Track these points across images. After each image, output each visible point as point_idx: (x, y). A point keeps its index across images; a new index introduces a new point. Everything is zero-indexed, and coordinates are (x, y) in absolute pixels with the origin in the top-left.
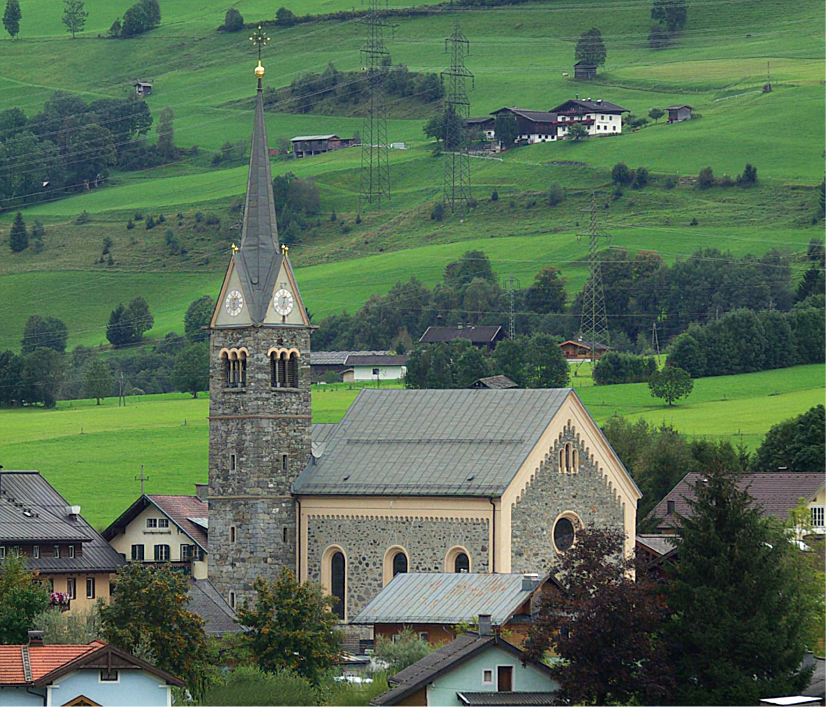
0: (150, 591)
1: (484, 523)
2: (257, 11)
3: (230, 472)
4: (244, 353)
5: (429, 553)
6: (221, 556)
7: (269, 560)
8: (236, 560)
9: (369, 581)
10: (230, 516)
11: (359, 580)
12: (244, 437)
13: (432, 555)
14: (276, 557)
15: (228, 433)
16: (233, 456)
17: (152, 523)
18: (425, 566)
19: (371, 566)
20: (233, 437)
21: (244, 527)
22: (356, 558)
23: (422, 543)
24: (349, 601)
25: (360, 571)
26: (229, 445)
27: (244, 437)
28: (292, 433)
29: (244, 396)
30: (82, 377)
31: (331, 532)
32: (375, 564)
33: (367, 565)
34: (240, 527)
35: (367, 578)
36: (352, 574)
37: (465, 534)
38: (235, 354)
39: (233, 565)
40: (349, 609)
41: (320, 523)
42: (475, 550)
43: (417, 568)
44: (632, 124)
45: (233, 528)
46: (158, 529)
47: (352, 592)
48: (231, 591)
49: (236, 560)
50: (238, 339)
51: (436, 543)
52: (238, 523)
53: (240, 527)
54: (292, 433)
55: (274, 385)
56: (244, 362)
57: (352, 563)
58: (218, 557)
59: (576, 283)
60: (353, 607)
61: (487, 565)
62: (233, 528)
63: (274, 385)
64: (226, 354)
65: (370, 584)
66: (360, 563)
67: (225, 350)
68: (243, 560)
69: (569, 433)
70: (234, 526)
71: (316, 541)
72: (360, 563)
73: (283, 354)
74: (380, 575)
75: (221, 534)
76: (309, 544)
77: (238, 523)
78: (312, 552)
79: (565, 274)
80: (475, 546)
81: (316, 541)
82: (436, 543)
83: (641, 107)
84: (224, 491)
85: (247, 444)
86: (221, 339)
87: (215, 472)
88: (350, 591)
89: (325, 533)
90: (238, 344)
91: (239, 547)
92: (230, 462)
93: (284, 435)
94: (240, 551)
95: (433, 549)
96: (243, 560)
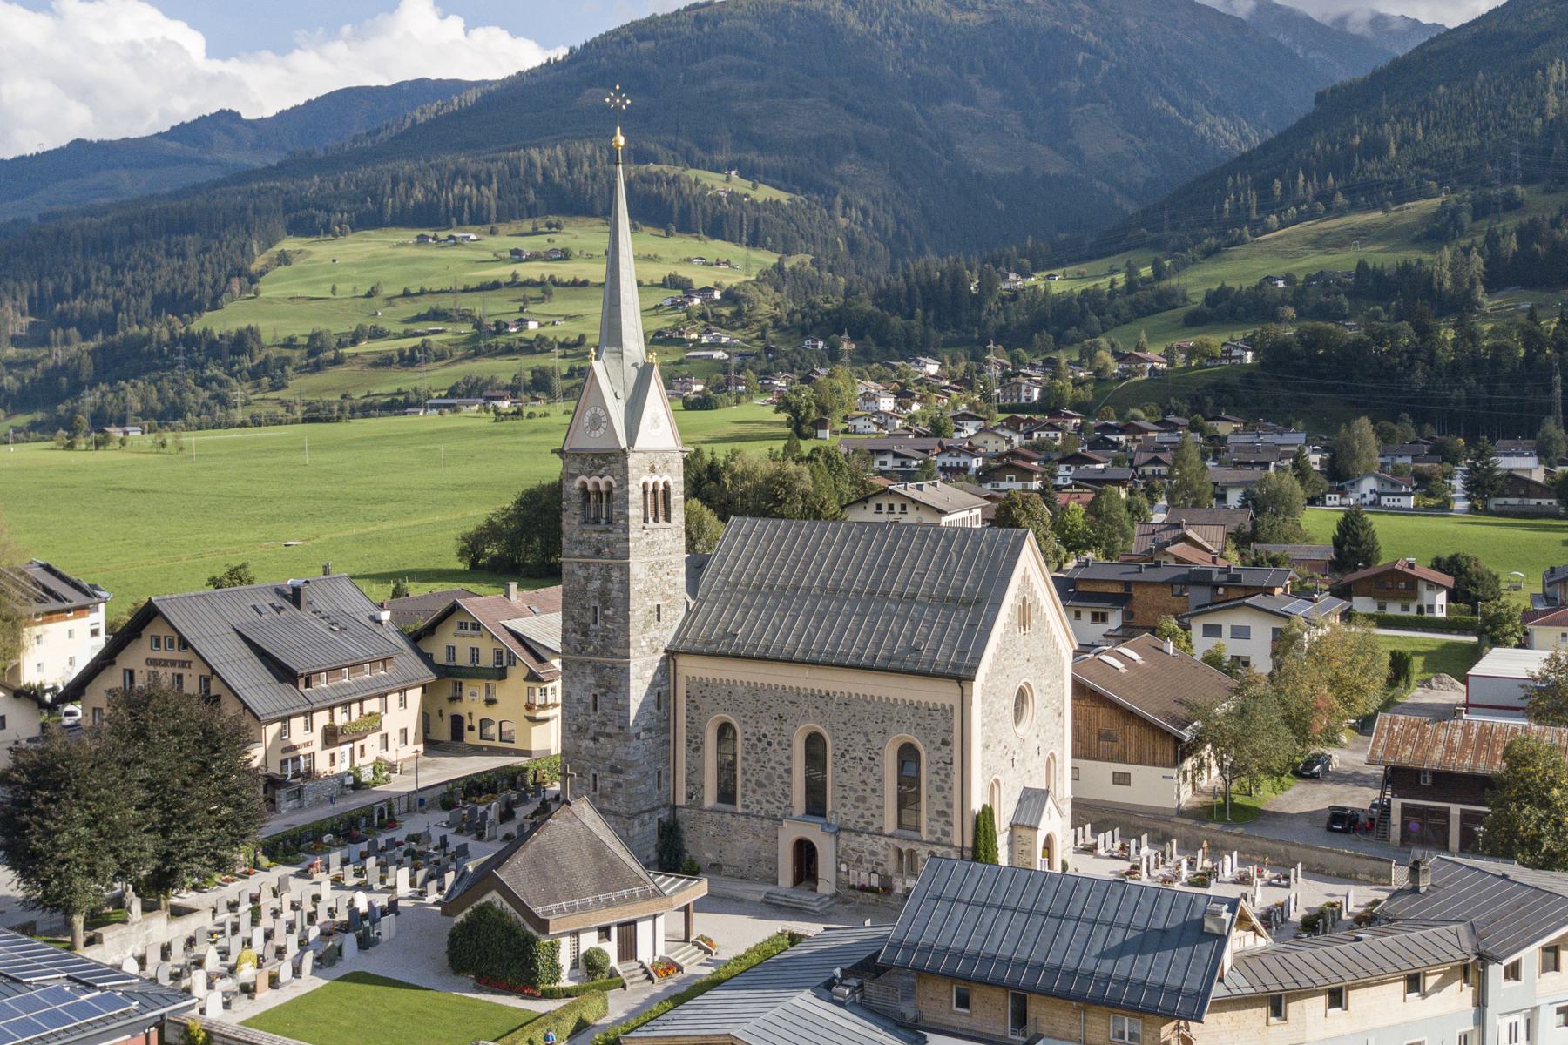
1: (946, 712)
3: (592, 626)
4: (609, 484)
5: (861, 739)
6: (579, 728)
7: (642, 735)
8: (601, 734)
9: (772, 764)
11: (758, 761)
14: (648, 730)
15: (588, 579)
17: (462, 626)
19: (775, 746)
21: (610, 695)
24: (744, 786)
26: (590, 594)
28: (666, 578)
30: (404, 807)
32: (780, 743)
33: (769, 744)
34: (604, 694)
37: (915, 721)
38: (597, 484)
39: (595, 739)
40: (744, 796)
43: (843, 755)
44: (541, 325)
46: (469, 631)
48: (593, 771)
49: (601, 734)
50: (600, 467)
51: (871, 727)
53: (604, 694)
54: (666, 578)
55: (646, 520)
56: (609, 493)
59: (610, 585)
60: (749, 793)
63: (646, 520)
64: (645, 485)
66: (759, 740)
67: (583, 478)
68: (609, 736)
71: (697, 708)
72: (759, 740)
73: (655, 484)
74: (789, 758)
78: (691, 721)
82: (871, 727)
83: (543, 320)
85: (614, 594)
88: (745, 773)
89: (709, 700)
90: (602, 472)
91: (604, 719)
92: (590, 614)
93: (657, 581)
94: (604, 724)
95: (866, 734)
96: (609, 736)
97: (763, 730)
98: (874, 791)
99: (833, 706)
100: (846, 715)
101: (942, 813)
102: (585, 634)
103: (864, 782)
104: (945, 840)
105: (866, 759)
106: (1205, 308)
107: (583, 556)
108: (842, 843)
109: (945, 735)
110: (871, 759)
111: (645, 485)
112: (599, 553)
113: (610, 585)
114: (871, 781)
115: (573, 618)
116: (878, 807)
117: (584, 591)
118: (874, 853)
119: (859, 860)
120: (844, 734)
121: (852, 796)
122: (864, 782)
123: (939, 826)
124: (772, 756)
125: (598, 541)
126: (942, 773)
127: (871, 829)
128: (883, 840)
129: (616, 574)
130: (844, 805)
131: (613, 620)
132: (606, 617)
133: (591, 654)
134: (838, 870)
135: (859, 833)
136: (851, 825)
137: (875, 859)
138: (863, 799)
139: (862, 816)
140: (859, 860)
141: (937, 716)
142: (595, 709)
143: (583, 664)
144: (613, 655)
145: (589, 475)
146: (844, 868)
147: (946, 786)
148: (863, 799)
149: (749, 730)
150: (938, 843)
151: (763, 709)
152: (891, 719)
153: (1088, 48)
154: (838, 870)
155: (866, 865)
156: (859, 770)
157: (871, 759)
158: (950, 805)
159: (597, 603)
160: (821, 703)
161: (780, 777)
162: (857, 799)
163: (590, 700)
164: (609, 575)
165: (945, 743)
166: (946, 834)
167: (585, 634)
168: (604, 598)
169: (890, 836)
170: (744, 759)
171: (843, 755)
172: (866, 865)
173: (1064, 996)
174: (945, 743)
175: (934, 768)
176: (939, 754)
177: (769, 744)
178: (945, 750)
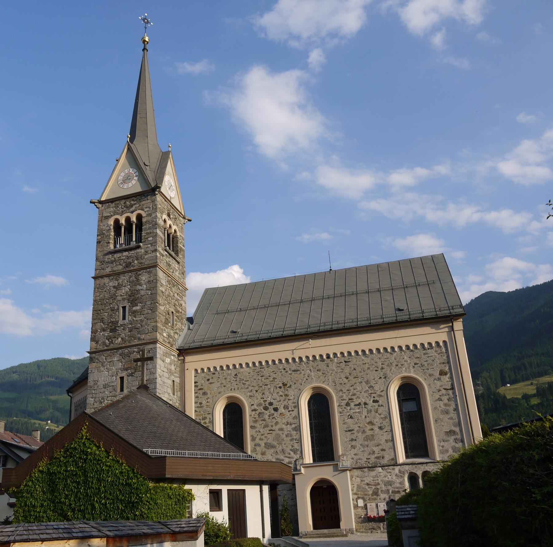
0: (534, 474)
2: (148, 47)
11: (266, 426)
12: (139, 287)
19: (281, 410)
20: (125, 290)
22: (260, 405)
23: (351, 378)
25: (267, 417)
26: (119, 298)
27: (139, 287)
29: (139, 250)
31: (224, 381)
32: (286, 407)
33: (276, 410)
34: (131, 375)
36: (256, 421)
38: (128, 219)
43: (348, 404)
45: (122, 379)
47: (257, 441)
50: (131, 206)
51: (372, 375)
57: (255, 410)
62: (122, 379)
64: (117, 222)
65: (281, 429)
66: (266, 408)
70: (124, 374)
71: (205, 394)
72: (266, 408)
73: (128, 219)
75: (105, 386)
80: (430, 371)
81: (205, 394)
82: (372, 375)
85: (142, 293)
87: (100, 325)
88: (253, 439)
95: (367, 382)
97: (269, 399)
99: (333, 366)
100: (347, 371)
102: (113, 330)
103: (371, 423)
105: (370, 402)
111: (117, 222)
114: (377, 421)
115: (102, 320)
117: (113, 297)
118: (390, 483)
120: (348, 387)
121: (361, 436)
124: (279, 420)
127: (385, 461)
128: (397, 469)
131: (141, 312)
132: (134, 313)
135: (372, 468)
138: (371, 438)
140: (376, 493)
145: (122, 214)
148: (371, 438)
149: (256, 402)
151: (267, 381)
155: (383, 496)
156: (365, 413)
157: (374, 401)
160: (322, 366)
162: (367, 438)
164: (138, 280)
167: (113, 330)
170: (252, 427)
173: (385, 290)
176: (438, 383)
177: (276, 410)
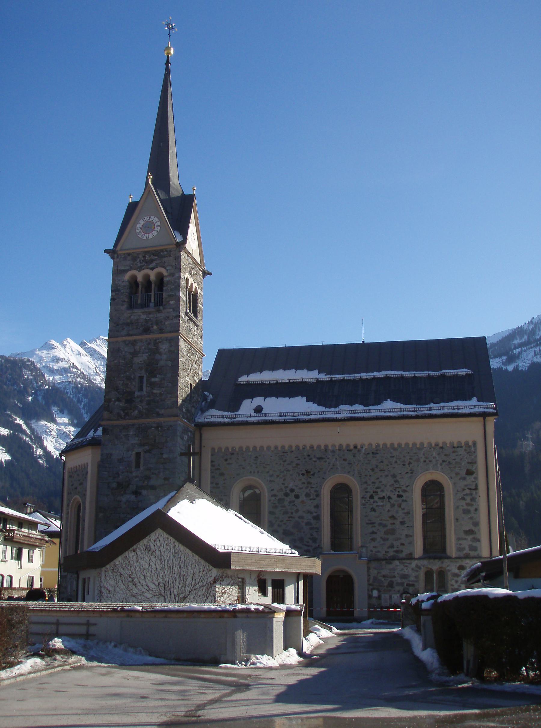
3: (137, 394)
9: (300, 513)
10: (135, 441)
11: (286, 513)
13: (392, 482)
15: (135, 354)
16: (141, 378)
18: (382, 495)
19: (303, 497)
32: (307, 495)
33: (297, 497)
34: (149, 451)
35: (297, 511)
41: (230, 455)
42: (457, 474)
43: (372, 497)
50: (152, 261)
52: (147, 447)
53: (149, 451)
58: (114, 485)
59: (158, 356)
61: (476, 489)
65: (301, 517)
66: (286, 495)
69: (250, 665)
70: (140, 450)
71: (222, 474)
72: (286, 495)
76: (213, 477)
77: (147, 447)
79: (153, 310)
81: (222, 474)
84: (127, 414)
85: (162, 363)
86: (128, 263)
95: (394, 476)
97: (291, 486)
98: (402, 523)
101: (470, 532)
104: (472, 554)
105: (394, 497)
106: (70, 391)
107: (129, 335)
108: (374, 572)
109: (469, 467)
110: (399, 496)
112: (147, 330)
113: (158, 356)
116: (407, 536)
118: (405, 576)
119: (391, 585)
122: (393, 517)
123: (466, 544)
125: (147, 321)
126: (468, 499)
129: (164, 347)
130: (373, 540)
132: (152, 385)
133: (136, 418)
134: (370, 597)
135: (390, 560)
136: (380, 555)
137: (406, 582)
138: (392, 532)
139: (392, 546)
140: (391, 585)
141: (461, 451)
142: (138, 466)
143: (126, 428)
144: (158, 415)
146: (375, 593)
147: (472, 509)
150: (467, 557)
152: (418, 460)
153: (172, 26)
154: (370, 597)
155: (397, 588)
157: (399, 496)
158: (476, 524)
159: (143, 373)
161: (308, 524)
163: (133, 458)
165: (469, 473)
166: (473, 548)
168: (152, 368)
169: (420, 559)
170: (271, 513)
171: (372, 497)
172: (397, 588)
174: (469, 473)
175: (460, 495)
176: (465, 483)
178: (470, 479)
